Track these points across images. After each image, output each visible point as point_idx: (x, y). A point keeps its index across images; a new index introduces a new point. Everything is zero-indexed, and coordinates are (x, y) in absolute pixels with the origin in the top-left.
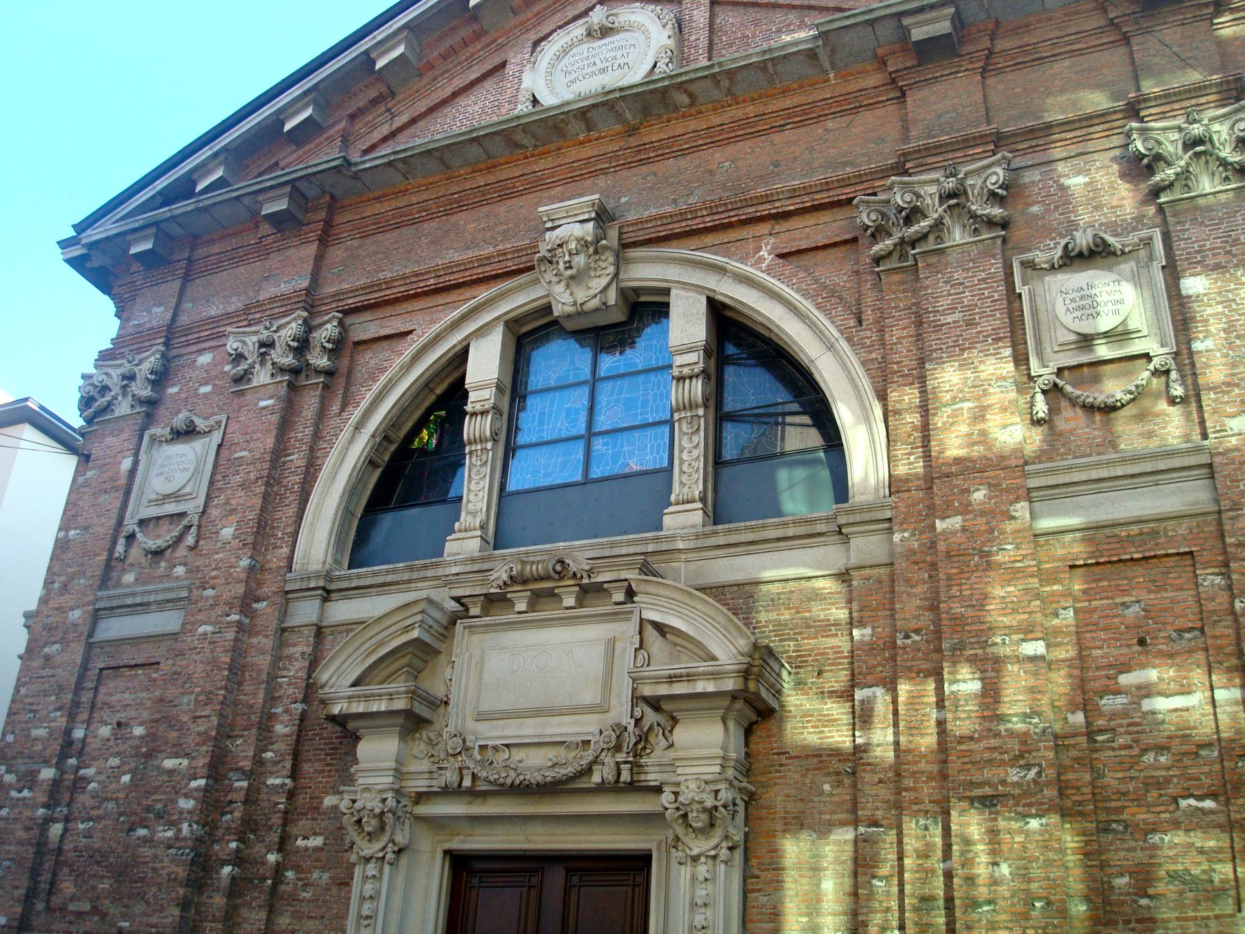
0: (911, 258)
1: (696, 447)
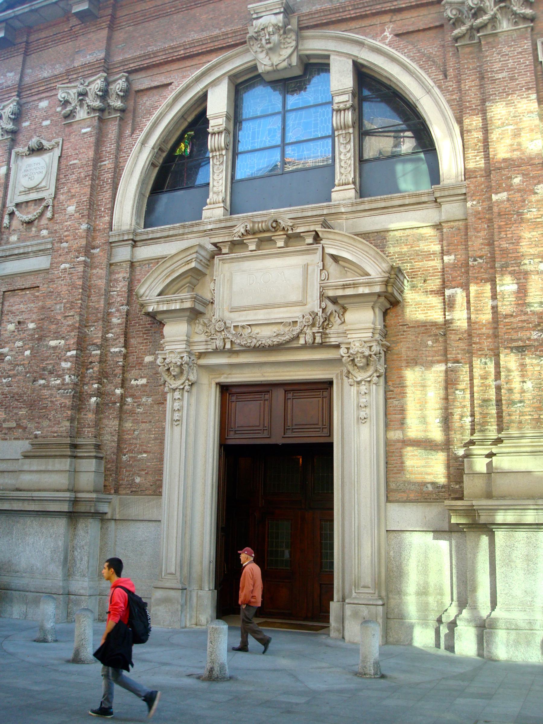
0: (476, 38)
1: (349, 152)
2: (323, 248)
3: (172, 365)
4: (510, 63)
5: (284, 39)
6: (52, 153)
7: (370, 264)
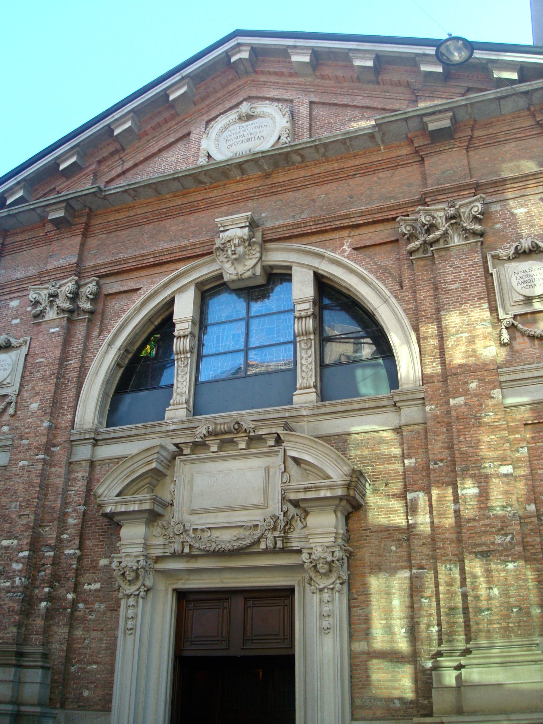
0: (430, 252)
1: (310, 356)
2: (285, 450)
3: (128, 569)
4: (462, 275)
5: (249, 250)
6: (19, 351)
7: (331, 467)
